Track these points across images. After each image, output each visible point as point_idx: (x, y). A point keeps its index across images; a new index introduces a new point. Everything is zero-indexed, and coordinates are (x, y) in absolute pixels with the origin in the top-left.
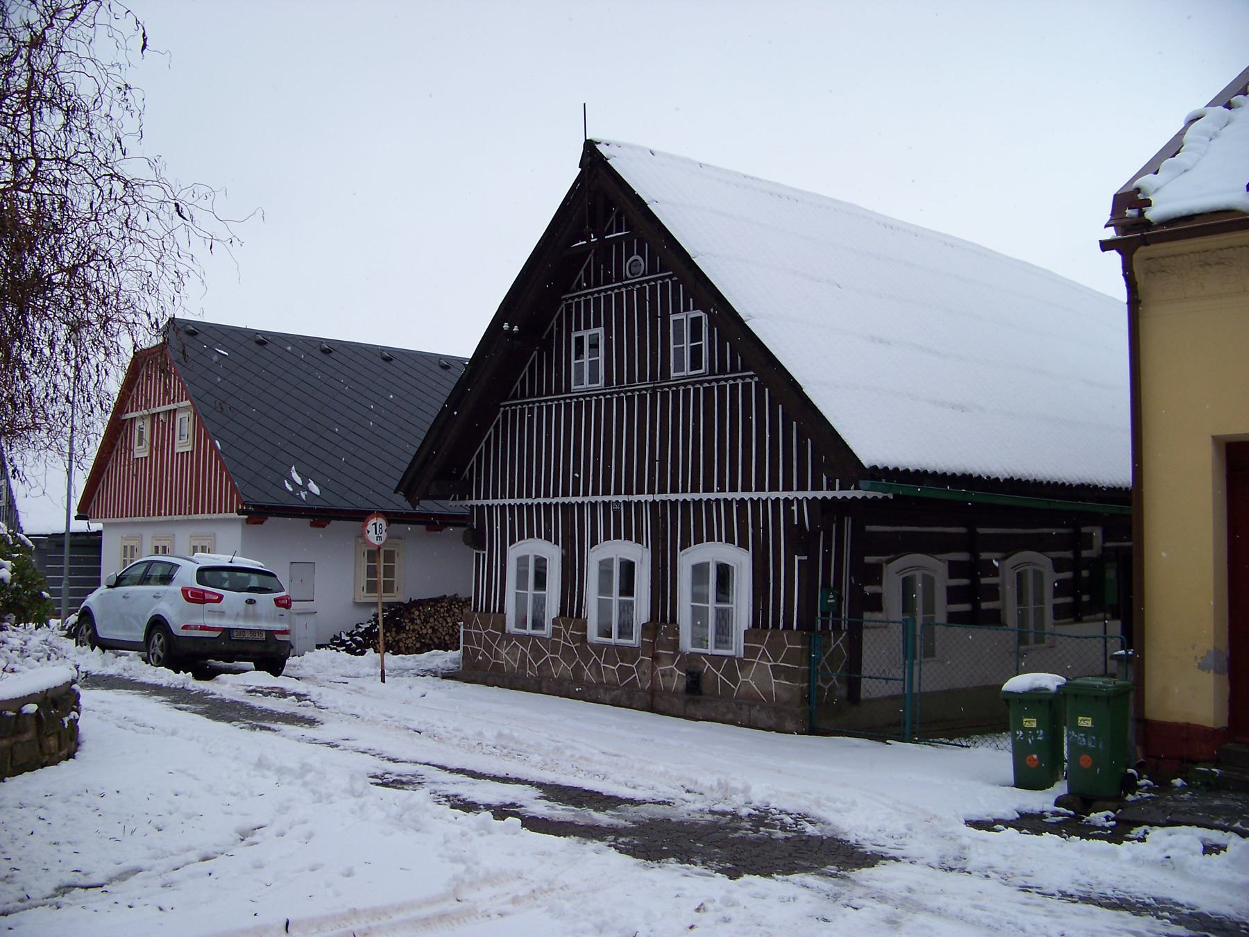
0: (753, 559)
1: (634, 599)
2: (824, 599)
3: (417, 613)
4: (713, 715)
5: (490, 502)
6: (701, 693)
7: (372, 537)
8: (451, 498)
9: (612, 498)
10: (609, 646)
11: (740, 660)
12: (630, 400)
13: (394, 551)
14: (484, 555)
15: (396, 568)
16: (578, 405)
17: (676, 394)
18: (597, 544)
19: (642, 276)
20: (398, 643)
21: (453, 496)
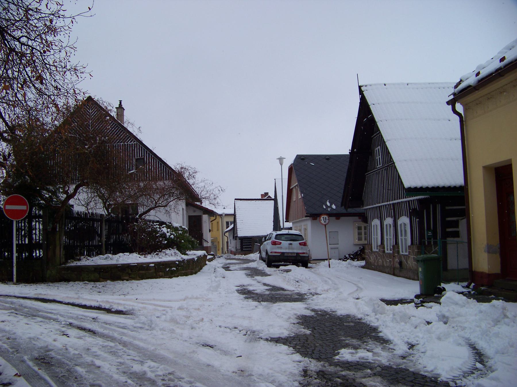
1: (407, 238)
7: (322, 222)
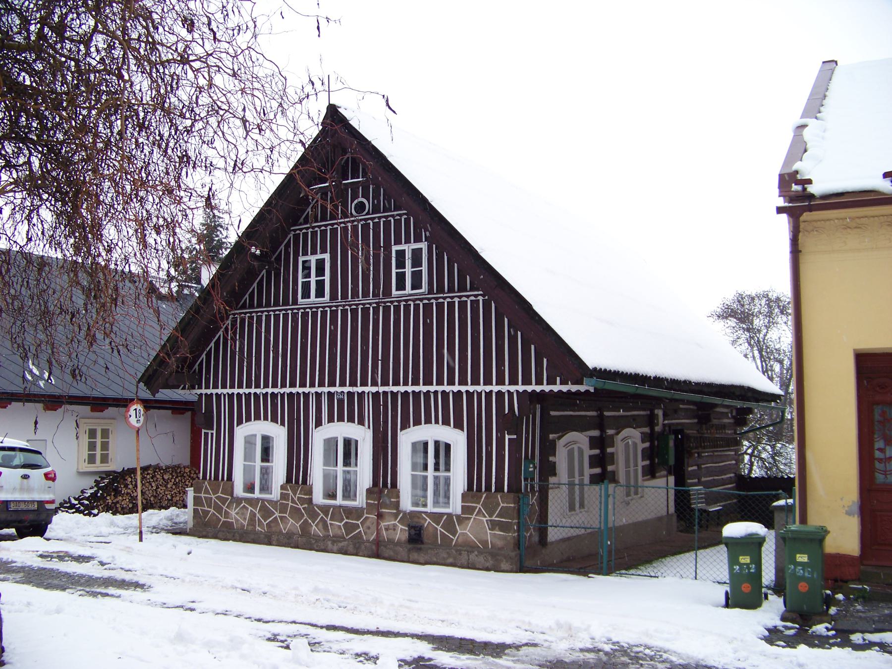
0: (467, 438)
2: (527, 468)
3: (130, 479)
4: (435, 559)
5: (220, 391)
6: (422, 543)
7: (133, 420)
8: (181, 388)
9: (337, 389)
10: (335, 507)
11: (458, 517)
12: (354, 312)
13: (108, 429)
14: (212, 434)
15: (110, 443)
16: (305, 315)
17: (397, 309)
18: (322, 425)
19: (367, 214)
20: (115, 505)
21: (182, 386)
